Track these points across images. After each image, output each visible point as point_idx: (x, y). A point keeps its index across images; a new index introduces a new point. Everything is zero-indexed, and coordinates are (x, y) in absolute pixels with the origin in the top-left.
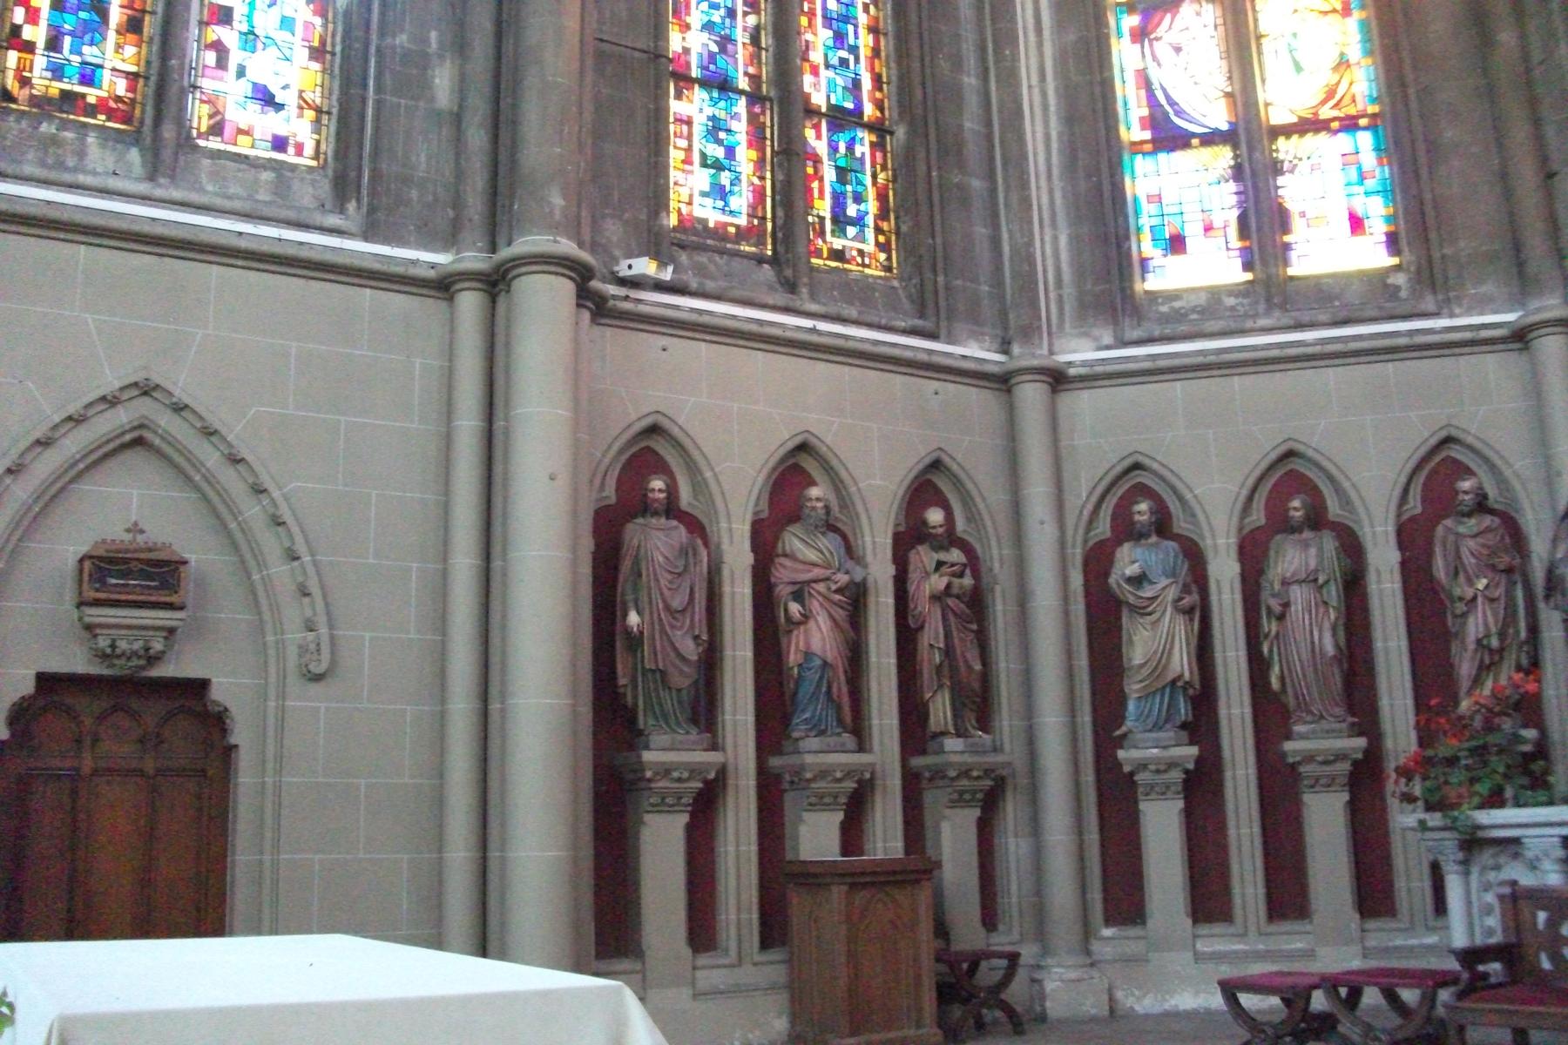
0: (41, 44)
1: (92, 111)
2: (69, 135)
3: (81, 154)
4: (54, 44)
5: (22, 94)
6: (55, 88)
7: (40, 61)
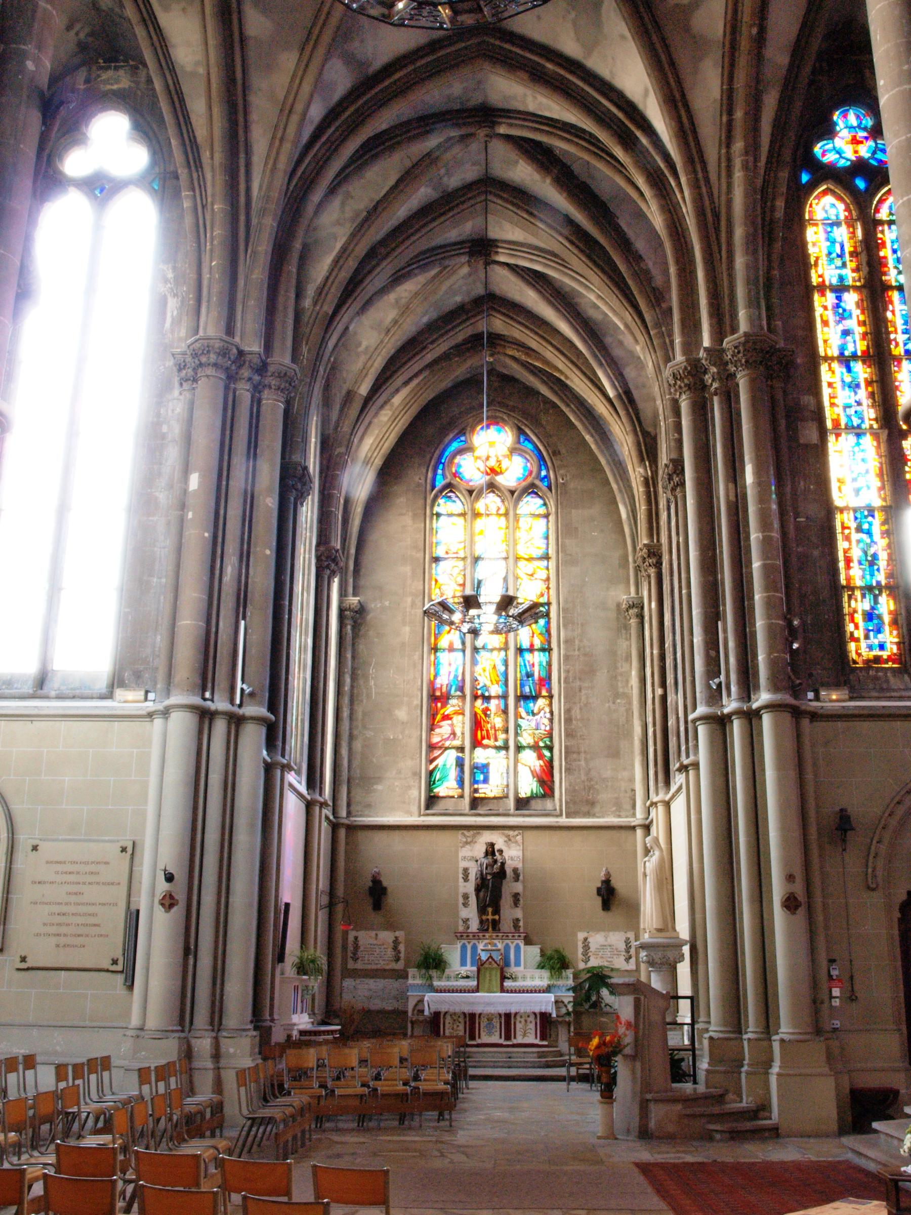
0: (862, 638)
1: (886, 661)
2: (880, 674)
3: (887, 681)
4: (867, 637)
5: (859, 660)
6: (872, 654)
7: (863, 644)
